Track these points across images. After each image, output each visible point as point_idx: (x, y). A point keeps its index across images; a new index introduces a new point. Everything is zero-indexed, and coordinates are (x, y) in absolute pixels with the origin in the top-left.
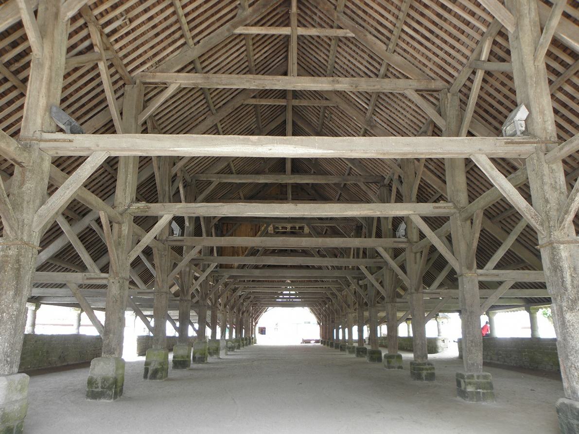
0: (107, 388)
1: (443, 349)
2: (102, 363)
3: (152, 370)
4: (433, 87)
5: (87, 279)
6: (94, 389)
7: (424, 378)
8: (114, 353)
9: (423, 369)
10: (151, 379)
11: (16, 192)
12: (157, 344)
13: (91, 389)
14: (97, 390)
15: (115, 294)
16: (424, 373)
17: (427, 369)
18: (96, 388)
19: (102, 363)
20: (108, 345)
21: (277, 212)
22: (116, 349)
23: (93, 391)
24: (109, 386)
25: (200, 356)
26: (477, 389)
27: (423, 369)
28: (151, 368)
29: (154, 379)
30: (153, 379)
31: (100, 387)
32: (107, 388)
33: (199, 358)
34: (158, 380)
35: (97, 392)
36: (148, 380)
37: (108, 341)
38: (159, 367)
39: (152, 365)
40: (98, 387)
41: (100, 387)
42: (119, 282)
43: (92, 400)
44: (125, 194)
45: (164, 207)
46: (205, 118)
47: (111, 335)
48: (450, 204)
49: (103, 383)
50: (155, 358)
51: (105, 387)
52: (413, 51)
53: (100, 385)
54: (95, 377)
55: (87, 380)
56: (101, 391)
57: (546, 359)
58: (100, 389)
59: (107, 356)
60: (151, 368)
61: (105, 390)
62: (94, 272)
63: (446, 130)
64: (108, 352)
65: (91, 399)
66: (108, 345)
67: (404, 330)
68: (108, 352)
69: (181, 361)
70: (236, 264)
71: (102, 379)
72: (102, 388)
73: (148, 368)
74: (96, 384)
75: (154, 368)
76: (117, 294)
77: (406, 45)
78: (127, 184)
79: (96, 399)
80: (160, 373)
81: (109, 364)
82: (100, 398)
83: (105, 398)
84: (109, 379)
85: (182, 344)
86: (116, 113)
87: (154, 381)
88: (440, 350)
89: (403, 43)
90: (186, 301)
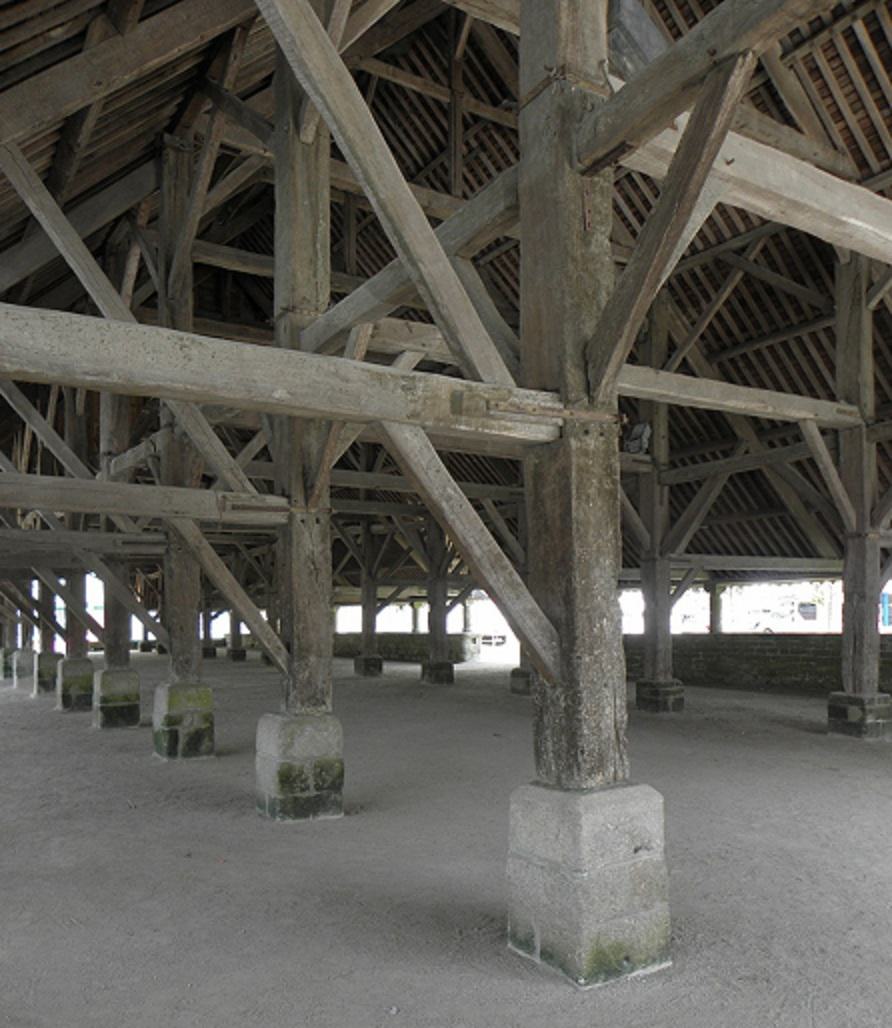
0: (328, 788)
1: (473, 654)
2: (309, 728)
3: (188, 734)
4: (841, 169)
5: (234, 508)
6: (299, 795)
7: (671, 708)
8: (324, 703)
9: (668, 693)
10: (186, 755)
11: (579, 253)
12: (187, 671)
13: (291, 795)
14: (306, 794)
15: (313, 553)
16: (671, 699)
17: (674, 693)
18: (303, 790)
19: (309, 728)
20: (309, 682)
21: (628, 383)
22: (327, 693)
23: (296, 799)
24: (333, 783)
25: (83, 692)
26: (877, 718)
27: (668, 693)
28: (186, 731)
29: (195, 755)
30: (191, 756)
31: (312, 787)
32: (328, 788)
33: (79, 698)
34: (205, 758)
35: (308, 800)
36: (179, 759)
37: (307, 674)
38: (203, 726)
39: (186, 723)
40: (308, 788)
41: (312, 787)
42: (318, 521)
43: (297, 821)
44: (315, 275)
45: (411, 331)
46: (835, 147)
47: (313, 659)
48: (854, 409)
49: (318, 775)
50: (191, 706)
51: (326, 785)
52: (833, 78)
53: (311, 782)
54: (297, 764)
55: (275, 774)
56: (317, 796)
57: (745, 666)
58: (313, 793)
59: (308, 710)
60: (184, 732)
61: (325, 792)
62: (245, 490)
63: (849, 264)
64: (309, 700)
65: (294, 819)
66: (309, 682)
67: (395, 620)
68: (309, 700)
69: (122, 708)
70: (240, 478)
71: (315, 767)
72: (318, 788)
73: (176, 732)
74: (302, 781)
75: (192, 729)
76: (316, 554)
77: (825, 61)
78: (318, 246)
79: (306, 816)
80: (206, 739)
81: (326, 730)
82: (315, 813)
83: (326, 811)
84: (333, 765)
85: (118, 668)
86: (375, 21)
87: (194, 759)
88: (468, 657)
89: (822, 55)
90: (122, 563)
